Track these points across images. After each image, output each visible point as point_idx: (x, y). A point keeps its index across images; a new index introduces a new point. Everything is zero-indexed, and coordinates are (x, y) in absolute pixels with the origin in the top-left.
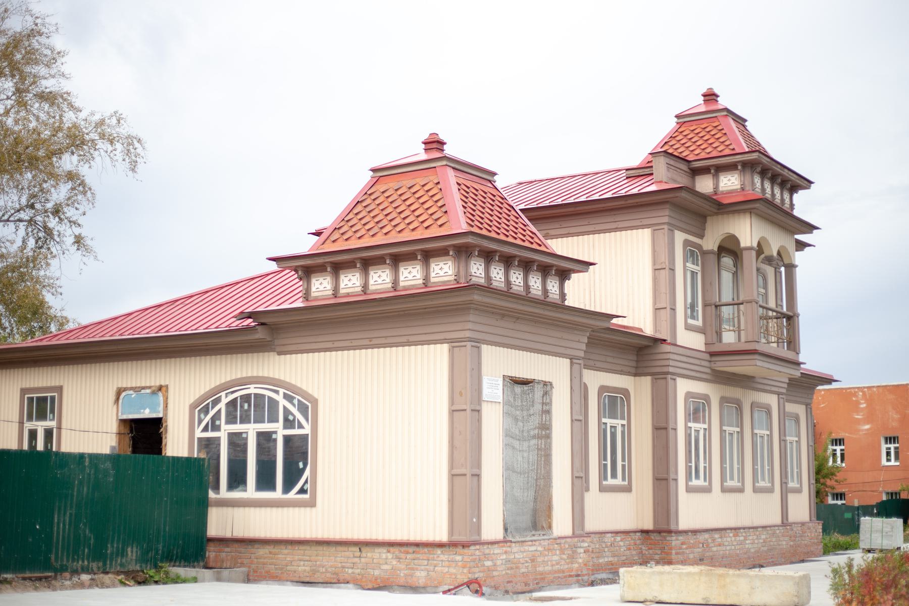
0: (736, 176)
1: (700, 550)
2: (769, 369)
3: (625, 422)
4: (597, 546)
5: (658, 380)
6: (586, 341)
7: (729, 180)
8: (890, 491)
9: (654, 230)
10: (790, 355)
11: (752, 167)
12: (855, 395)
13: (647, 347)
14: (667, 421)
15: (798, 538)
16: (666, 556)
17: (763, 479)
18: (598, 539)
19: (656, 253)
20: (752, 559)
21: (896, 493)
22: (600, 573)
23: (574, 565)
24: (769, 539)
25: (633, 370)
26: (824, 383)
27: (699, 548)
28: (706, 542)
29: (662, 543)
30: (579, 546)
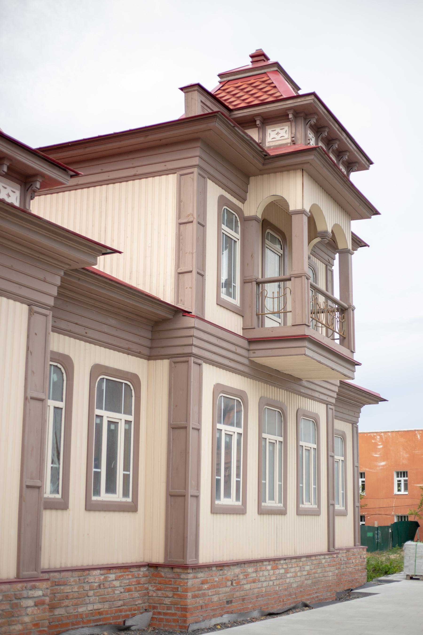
0: (286, 128)
1: (228, 589)
2: (320, 362)
3: (131, 418)
4: (76, 589)
5: (177, 365)
6: (59, 283)
7: (278, 133)
8: (400, 514)
9: (181, 175)
10: (344, 351)
11: (305, 119)
12: (374, 438)
13: (165, 320)
14: (187, 419)
15: (343, 566)
16: (179, 600)
17: (309, 500)
18: (77, 579)
19: (182, 204)
20: (294, 596)
21: (405, 517)
22: (78, 628)
23: (12, 627)
24: (314, 571)
25: (146, 351)
26: (371, 401)
27: (226, 587)
28: (236, 578)
29: (175, 582)
30: (25, 596)
